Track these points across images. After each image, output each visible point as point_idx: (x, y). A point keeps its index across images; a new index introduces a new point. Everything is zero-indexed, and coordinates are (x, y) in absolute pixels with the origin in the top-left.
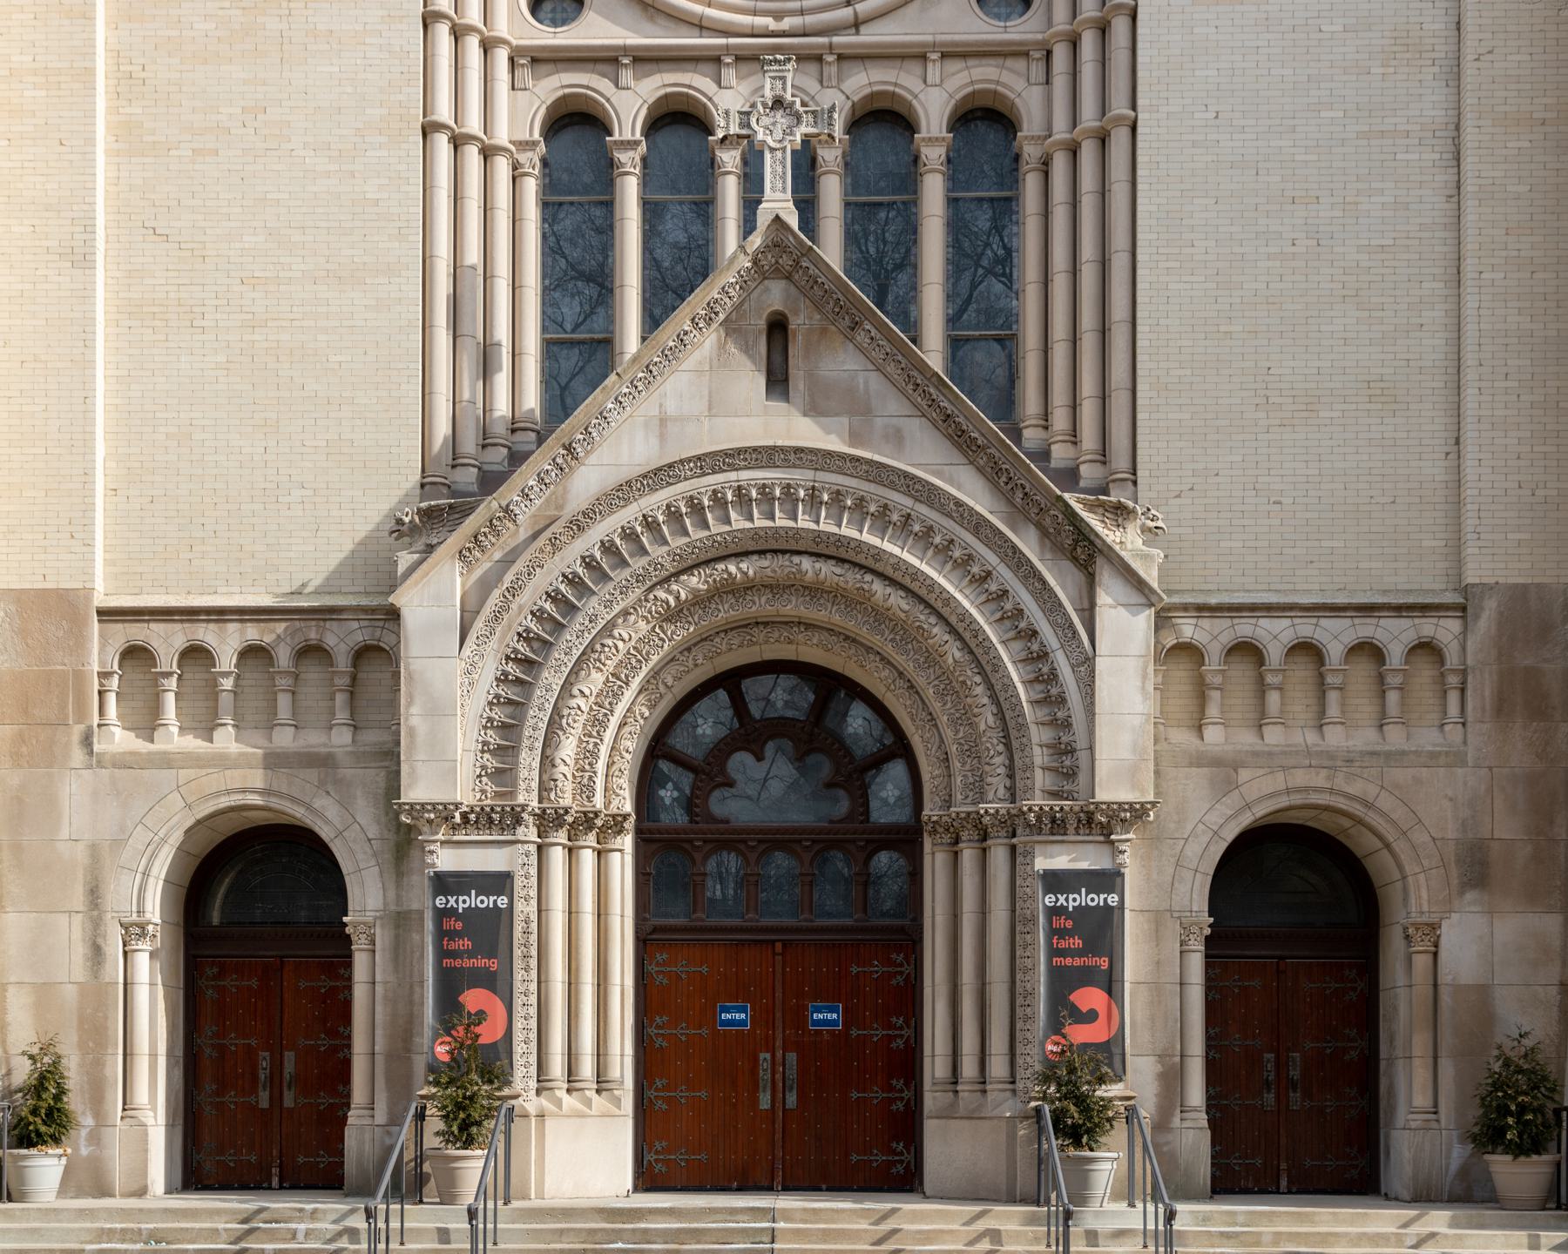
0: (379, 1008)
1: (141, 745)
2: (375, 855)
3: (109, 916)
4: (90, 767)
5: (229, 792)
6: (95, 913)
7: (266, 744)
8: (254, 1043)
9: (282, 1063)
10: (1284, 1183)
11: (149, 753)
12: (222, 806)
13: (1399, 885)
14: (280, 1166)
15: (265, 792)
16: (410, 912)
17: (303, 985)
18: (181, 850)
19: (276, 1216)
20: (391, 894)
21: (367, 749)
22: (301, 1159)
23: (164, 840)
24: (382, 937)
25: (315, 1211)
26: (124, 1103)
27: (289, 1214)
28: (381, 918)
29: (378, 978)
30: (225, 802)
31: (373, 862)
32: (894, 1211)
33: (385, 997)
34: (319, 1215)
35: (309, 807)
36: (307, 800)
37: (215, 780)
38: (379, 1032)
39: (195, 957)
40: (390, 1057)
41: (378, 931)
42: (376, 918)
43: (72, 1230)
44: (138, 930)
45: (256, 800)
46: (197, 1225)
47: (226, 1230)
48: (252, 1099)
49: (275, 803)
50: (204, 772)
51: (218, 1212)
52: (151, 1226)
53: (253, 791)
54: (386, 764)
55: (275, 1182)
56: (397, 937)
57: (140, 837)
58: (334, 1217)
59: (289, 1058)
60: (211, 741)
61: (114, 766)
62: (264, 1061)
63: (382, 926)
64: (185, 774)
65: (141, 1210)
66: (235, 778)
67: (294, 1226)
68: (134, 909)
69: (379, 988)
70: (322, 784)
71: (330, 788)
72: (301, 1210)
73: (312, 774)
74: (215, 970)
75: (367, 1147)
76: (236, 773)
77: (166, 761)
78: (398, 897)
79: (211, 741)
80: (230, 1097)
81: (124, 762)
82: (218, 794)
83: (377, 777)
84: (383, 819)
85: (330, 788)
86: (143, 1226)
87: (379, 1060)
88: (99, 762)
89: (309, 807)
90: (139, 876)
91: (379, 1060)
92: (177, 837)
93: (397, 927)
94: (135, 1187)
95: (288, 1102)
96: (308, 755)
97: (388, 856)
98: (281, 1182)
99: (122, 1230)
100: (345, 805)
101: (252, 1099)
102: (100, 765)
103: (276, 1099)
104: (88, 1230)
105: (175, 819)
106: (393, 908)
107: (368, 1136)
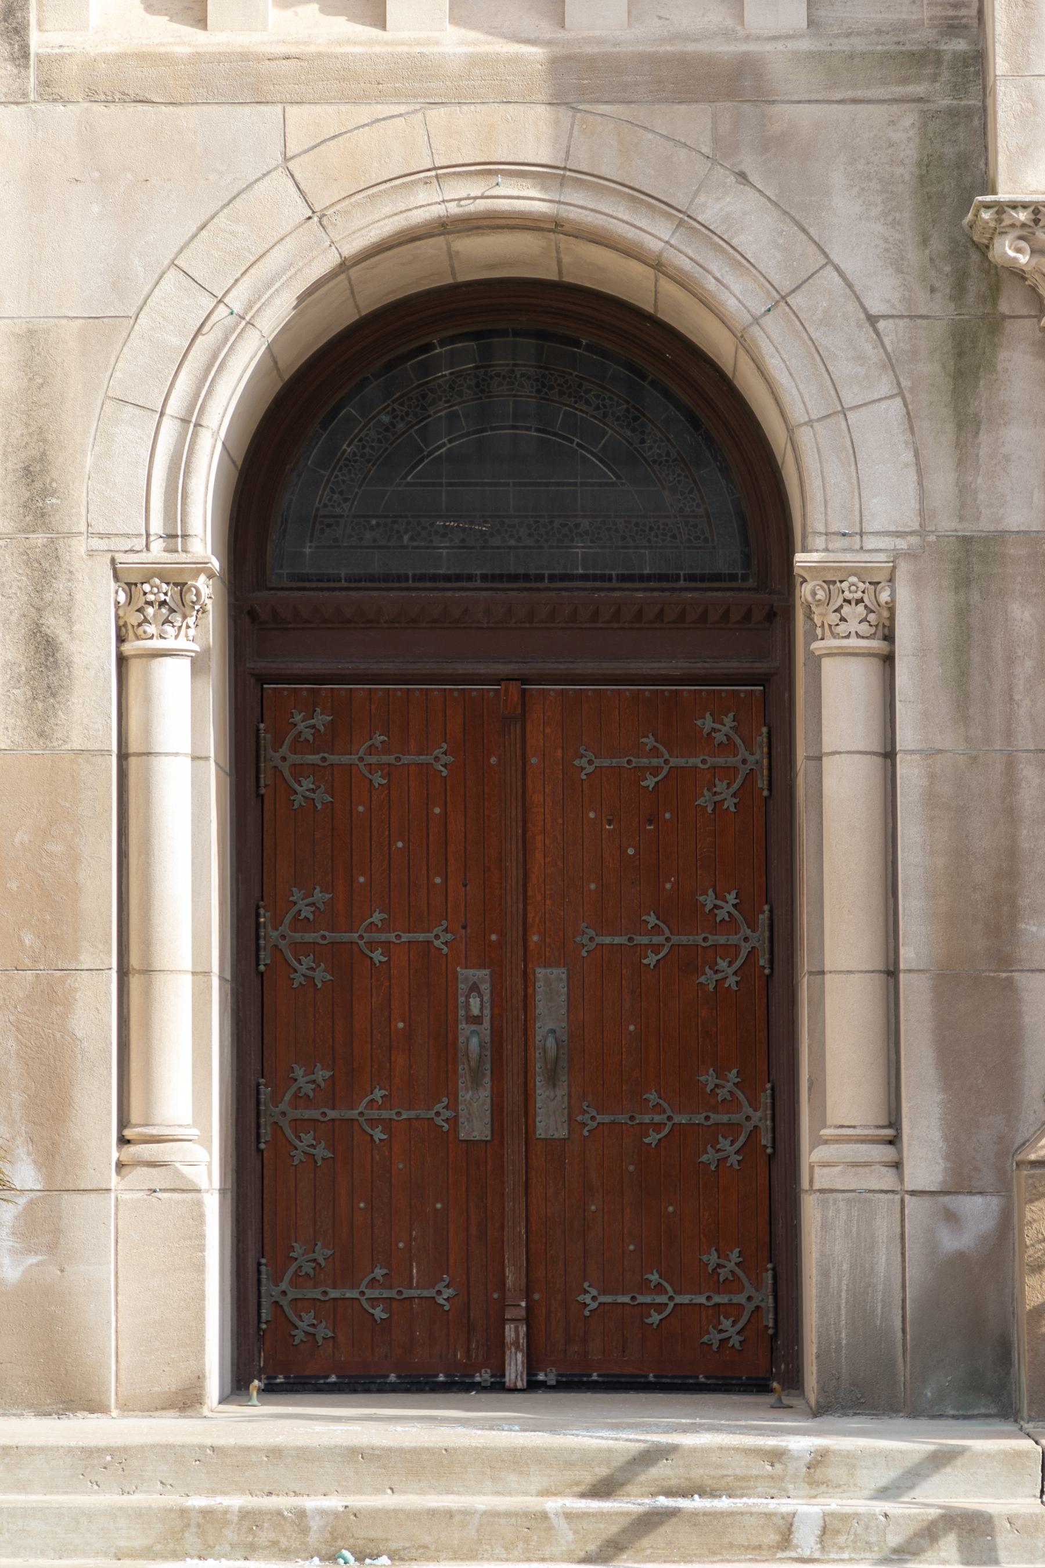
0: (911, 832)
1: (339, 34)
2: (890, 363)
3: (80, 546)
4: (20, 99)
5: (439, 174)
6: (39, 539)
7: (546, 30)
8: (440, 938)
9: (527, 1002)
10: (515, 1368)
11: (198, 58)
12: (419, 216)
13: (667, 287)
14: (529, 1319)
15: (556, 175)
16: (1001, 537)
17: (586, 765)
18: (271, 352)
19: (698, 1474)
20: (943, 482)
21: (860, 44)
22: (591, 1298)
23: (245, 320)
24: (919, 618)
25: (819, 1459)
26: (123, 1122)
27: (738, 1466)
28: (911, 555)
29: (906, 737)
30: (427, 205)
31: (884, 386)
32: (649, 1457)
33: (930, 798)
34: (832, 1473)
35: (684, 220)
36: (680, 200)
37: (398, 139)
38: (912, 907)
39: (262, 679)
40: (952, 981)
41: (904, 597)
42: (897, 556)
43: (89, 1514)
44: (165, 592)
45: (527, 198)
46: (482, 1502)
47: (570, 1516)
48: (439, 1113)
49: (581, 207)
50: (364, 113)
51: (518, 1460)
52: (334, 1502)
53: (518, 170)
54: (919, 89)
55: (515, 1368)
56: (962, 613)
57: (173, 309)
58: (884, 1476)
59: (551, 987)
60: (381, 22)
61: (92, 95)
62: (474, 992)
63: (918, 581)
64: (306, 121)
65: (275, 1453)
66: (458, 132)
67: (783, 1505)
68: (157, 526)
69: (908, 770)
70: (723, 150)
71: (748, 162)
72: (776, 1456)
73: (694, 122)
74: (321, 720)
75: (884, 1260)
76: (464, 117)
77: (248, 81)
78: (964, 491)
79: (381, 22)
80: (371, 1108)
81: (122, 85)
82: (406, 180)
83: (890, 131)
84: (914, 257)
85: (748, 162)
86: (311, 1503)
87: (916, 995)
88: (45, 83)
89: (684, 220)
90: (169, 429)
91: (916, 995)
92: (276, 314)
93: (962, 582)
94: (169, 1382)
95: (550, 1118)
96: (682, 61)
97: (929, 368)
98: (532, 1366)
99: (245, 1514)
100: (795, 213)
101: (439, 1113)
102: (50, 91)
103: (512, 1112)
104: (138, 1514)
105: (278, 257)
106: (947, 524)
107: (884, 1227)
